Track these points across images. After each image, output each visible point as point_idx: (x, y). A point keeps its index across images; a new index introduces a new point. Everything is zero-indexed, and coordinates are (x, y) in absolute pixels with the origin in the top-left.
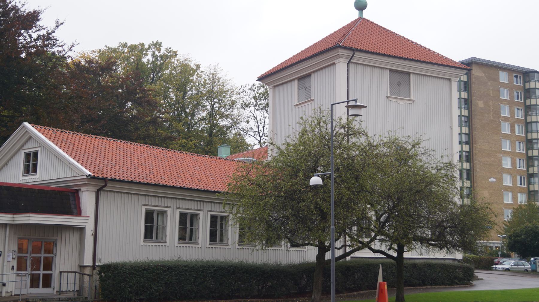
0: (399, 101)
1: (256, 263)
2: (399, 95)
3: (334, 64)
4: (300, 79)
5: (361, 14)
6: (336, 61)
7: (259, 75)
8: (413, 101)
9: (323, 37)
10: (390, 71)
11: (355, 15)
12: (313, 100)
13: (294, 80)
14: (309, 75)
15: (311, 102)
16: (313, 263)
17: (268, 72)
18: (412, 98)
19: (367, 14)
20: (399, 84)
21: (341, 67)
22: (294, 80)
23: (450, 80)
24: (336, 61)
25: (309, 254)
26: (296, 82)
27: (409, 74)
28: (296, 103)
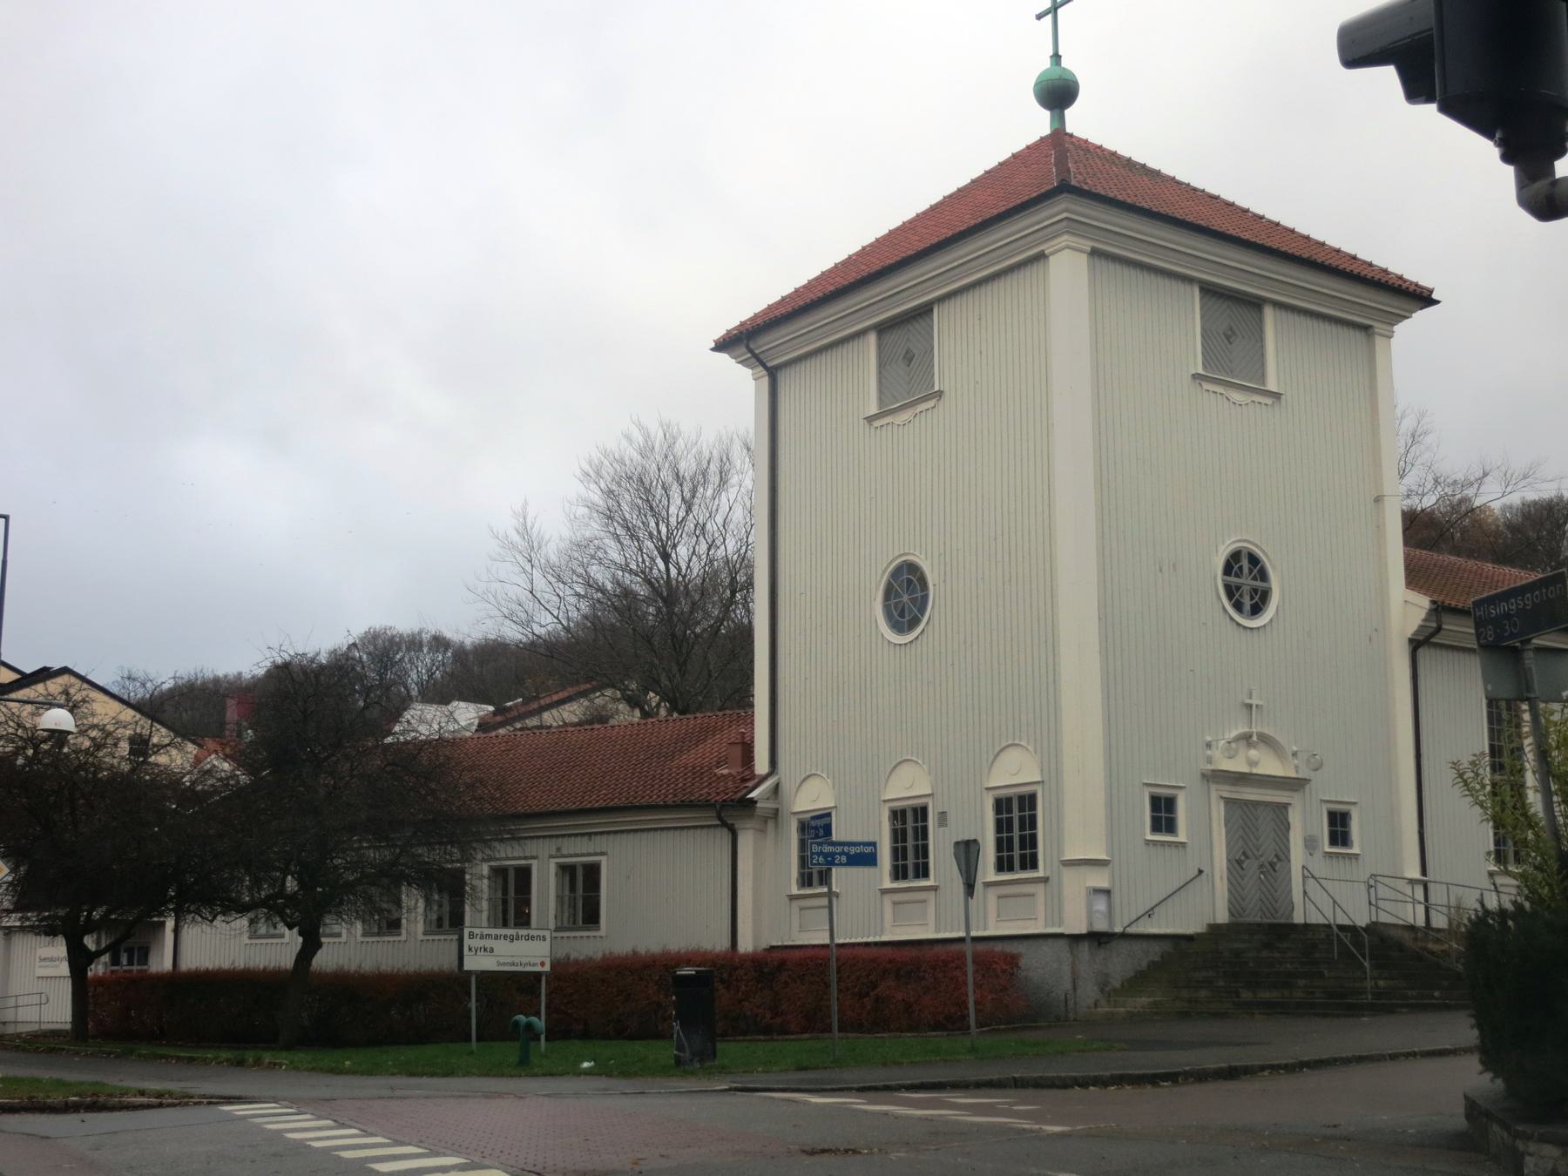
0: (1237, 396)
1: (635, 953)
2: (1231, 372)
3: (1041, 257)
4: (882, 329)
5: (1059, 119)
6: (1047, 248)
7: (719, 333)
8: (1277, 396)
9: (947, 193)
10: (1202, 289)
11: (1039, 123)
12: (940, 394)
13: (862, 333)
14: (925, 311)
15: (931, 404)
16: (286, 971)
17: (751, 319)
18: (1272, 385)
19: (1078, 121)
20: (1229, 336)
21: (1068, 271)
22: (862, 333)
23: (1366, 329)
24: (1047, 248)
25: (277, 949)
26: (872, 338)
27: (1255, 304)
28: (874, 410)
